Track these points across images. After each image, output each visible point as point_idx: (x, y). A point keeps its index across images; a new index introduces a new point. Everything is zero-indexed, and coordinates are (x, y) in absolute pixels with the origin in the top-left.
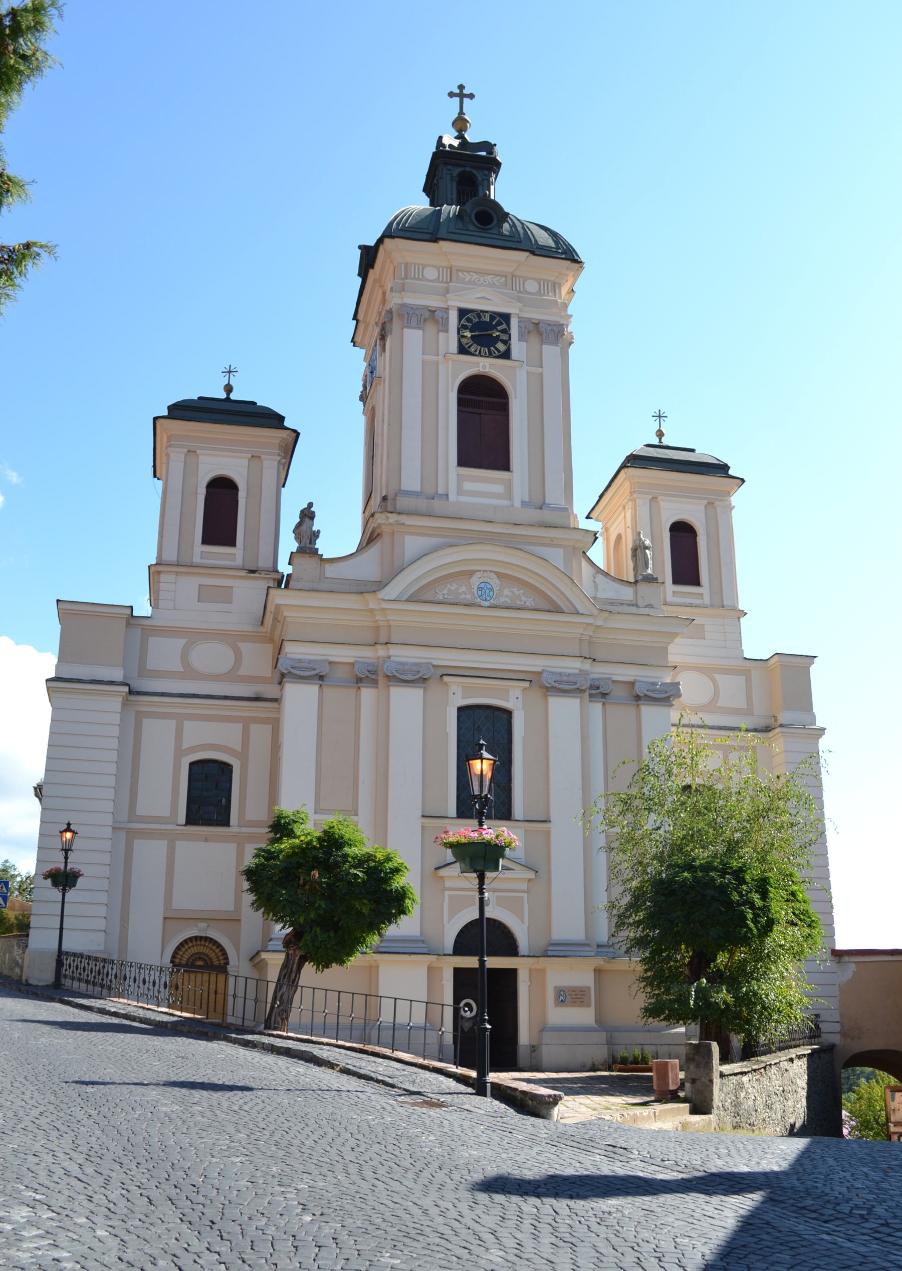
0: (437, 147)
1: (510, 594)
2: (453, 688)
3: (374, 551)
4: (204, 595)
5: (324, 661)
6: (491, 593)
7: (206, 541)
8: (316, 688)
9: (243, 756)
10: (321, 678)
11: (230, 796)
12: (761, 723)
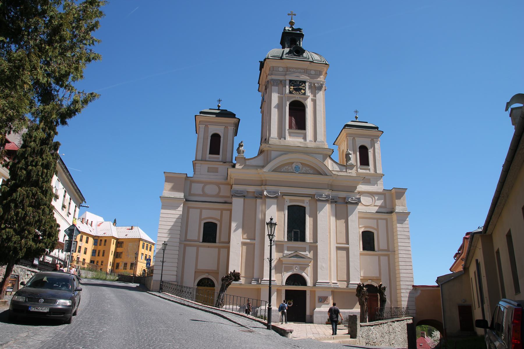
3: (261, 156)
4: (210, 170)
9: (377, 229)
12: (390, 210)
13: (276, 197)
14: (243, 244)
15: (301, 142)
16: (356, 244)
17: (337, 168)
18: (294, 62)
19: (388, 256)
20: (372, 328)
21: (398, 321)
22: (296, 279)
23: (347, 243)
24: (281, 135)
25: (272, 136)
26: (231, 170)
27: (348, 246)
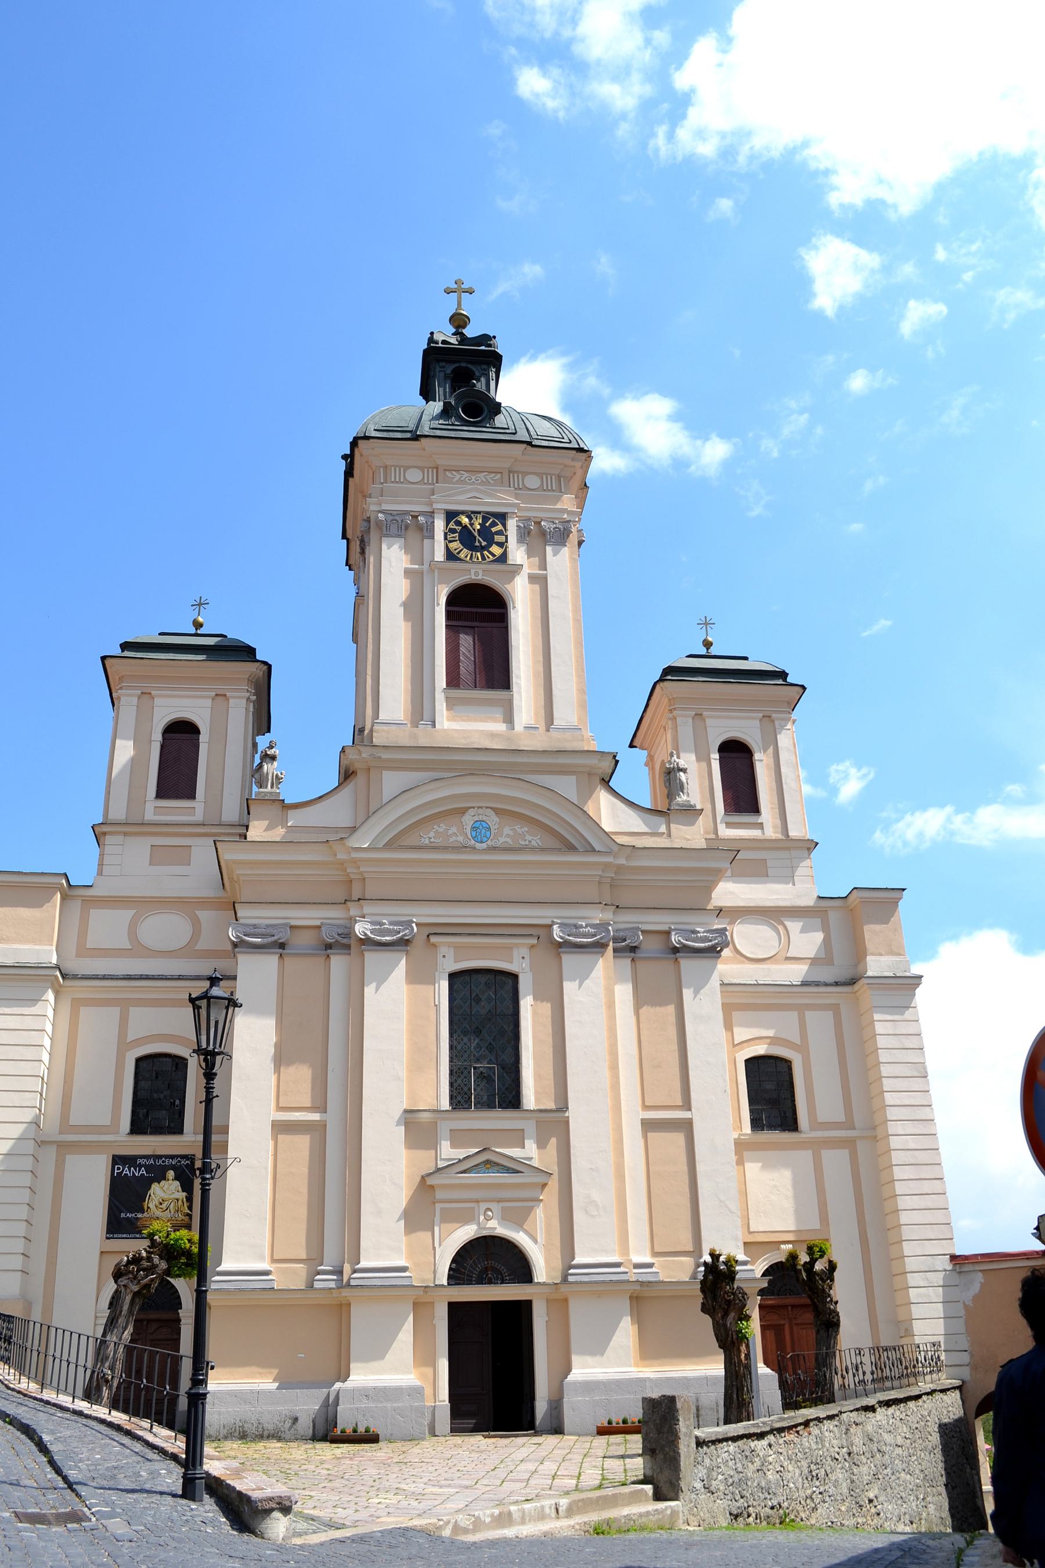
0: (428, 344)
1: (511, 833)
2: (443, 950)
3: (347, 791)
5: (285, 925)
6: (488, 833)
7: (161, 794)
8: (275, 959)
9: (803, 1048)
10: (282, 946)
11: (184, 1097)
12: (844, 975)
13: (403, 943)
14: (280, 1128)
15: (493, 735)
16: (722, 1104)
17: (634, 822)
18: (465, 450)
19: (849, 1144)
20: (760, 1445)
21: (888, 1404)
22: (491, 1258)
23: (687, 1105)
24: (421, 710)
25: (383, 716)
26: (231, 853)
27: (686, 1115)
